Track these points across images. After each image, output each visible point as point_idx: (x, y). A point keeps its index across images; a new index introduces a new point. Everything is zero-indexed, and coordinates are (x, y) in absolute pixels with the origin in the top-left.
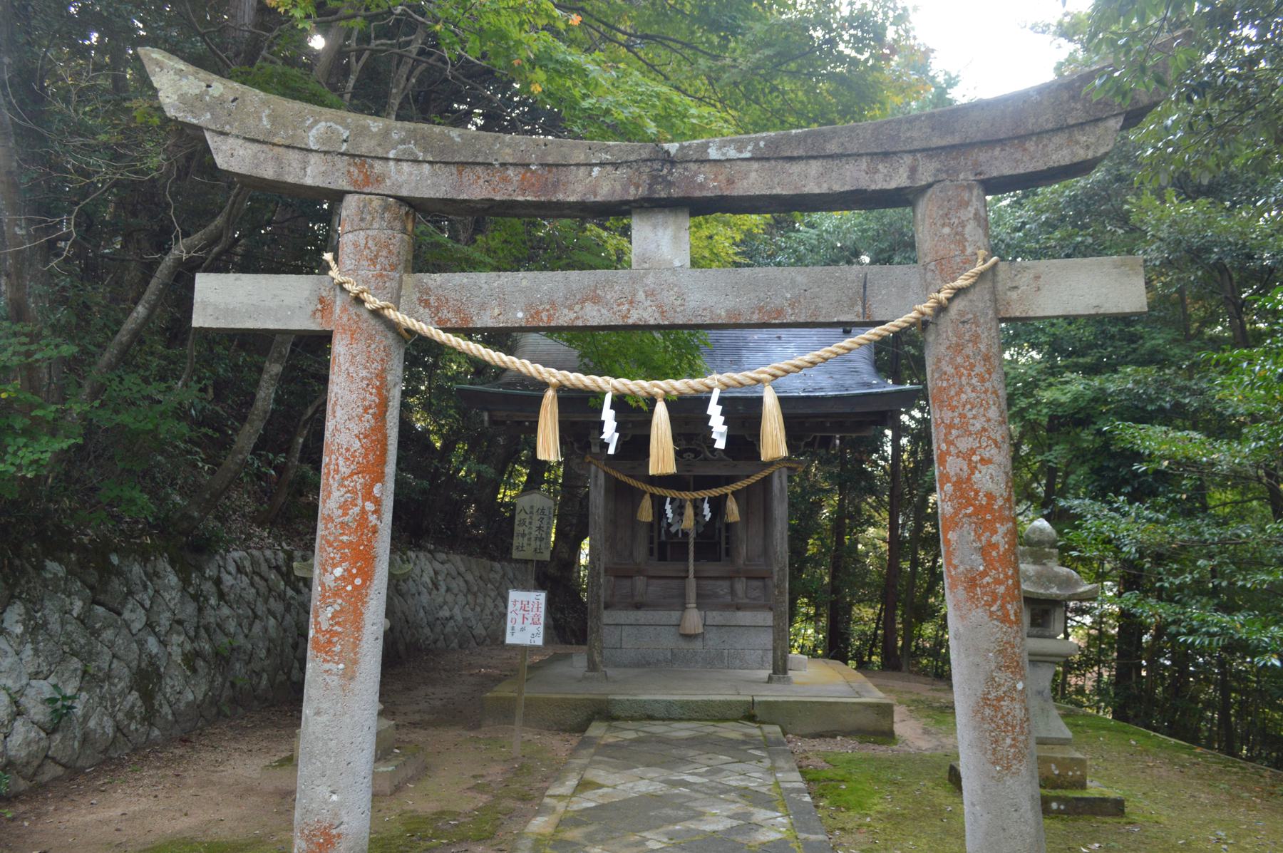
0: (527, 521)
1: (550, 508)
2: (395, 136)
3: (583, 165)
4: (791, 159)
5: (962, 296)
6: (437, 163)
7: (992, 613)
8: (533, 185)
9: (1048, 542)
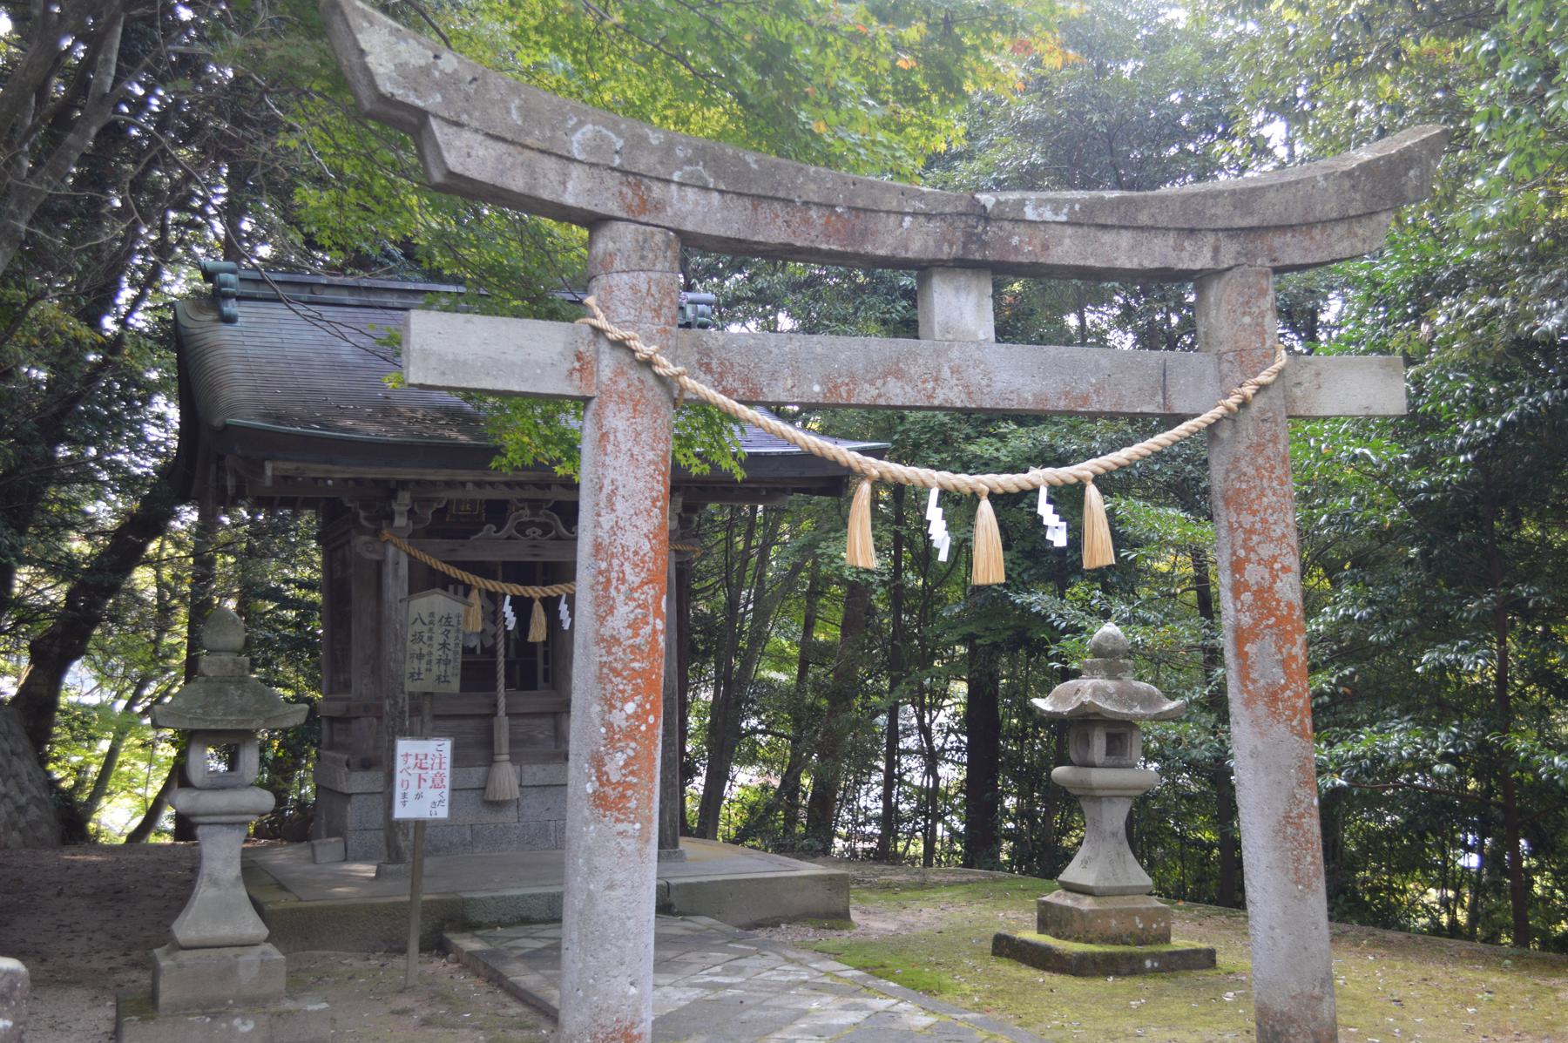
0: (426, 635)
1: (458, 616)
2: (680, 154)
3: (895, 213)
4: (1104, 227)
5: (1263, 392)
6: (728, 192)
7: (1293, 727)
8: (838, 231)
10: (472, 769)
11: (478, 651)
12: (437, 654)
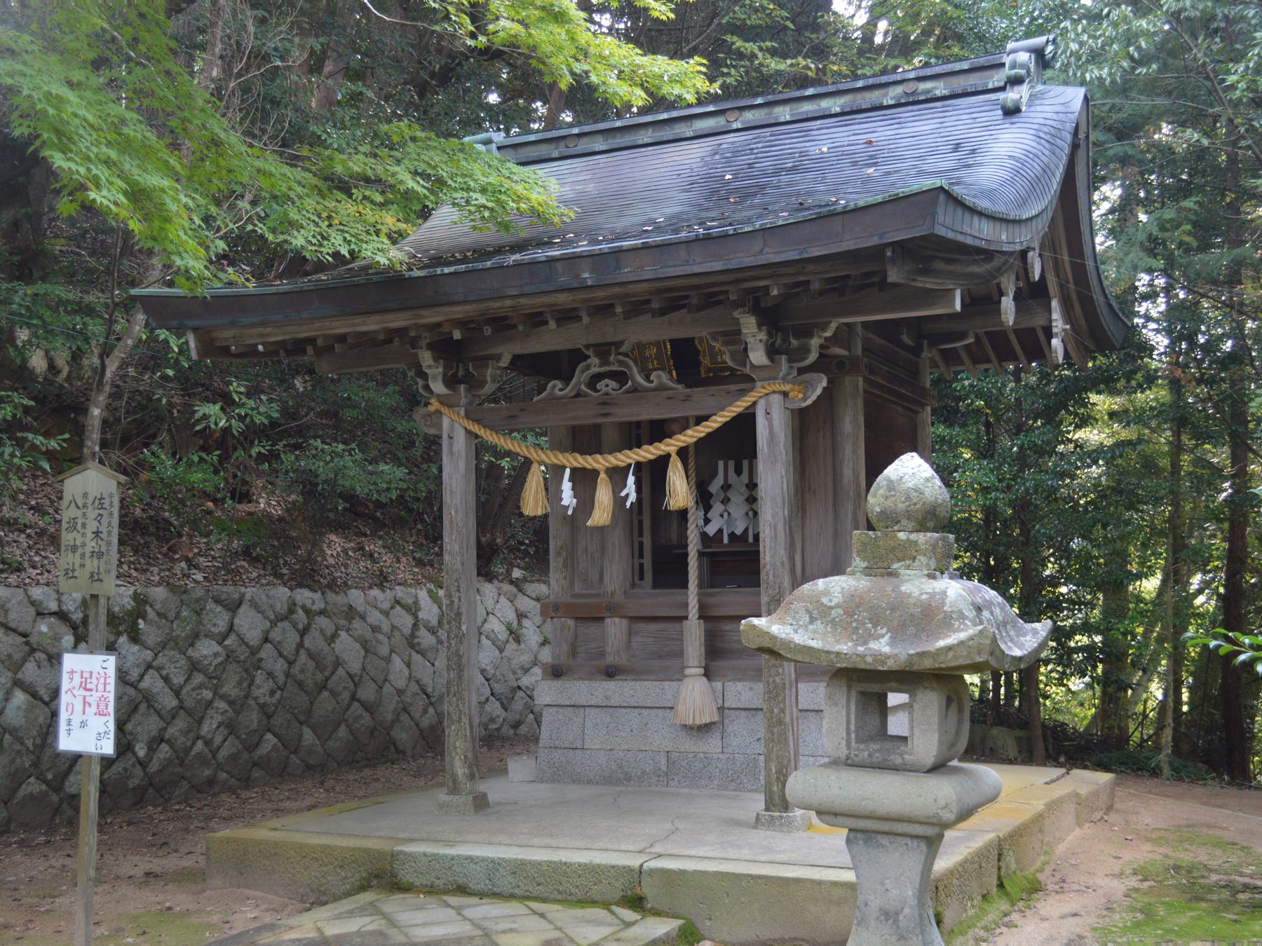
0: (80, 521)
9: (908, 515)
10: (666, 683)
11: (726, 540)
12: (91, 545)
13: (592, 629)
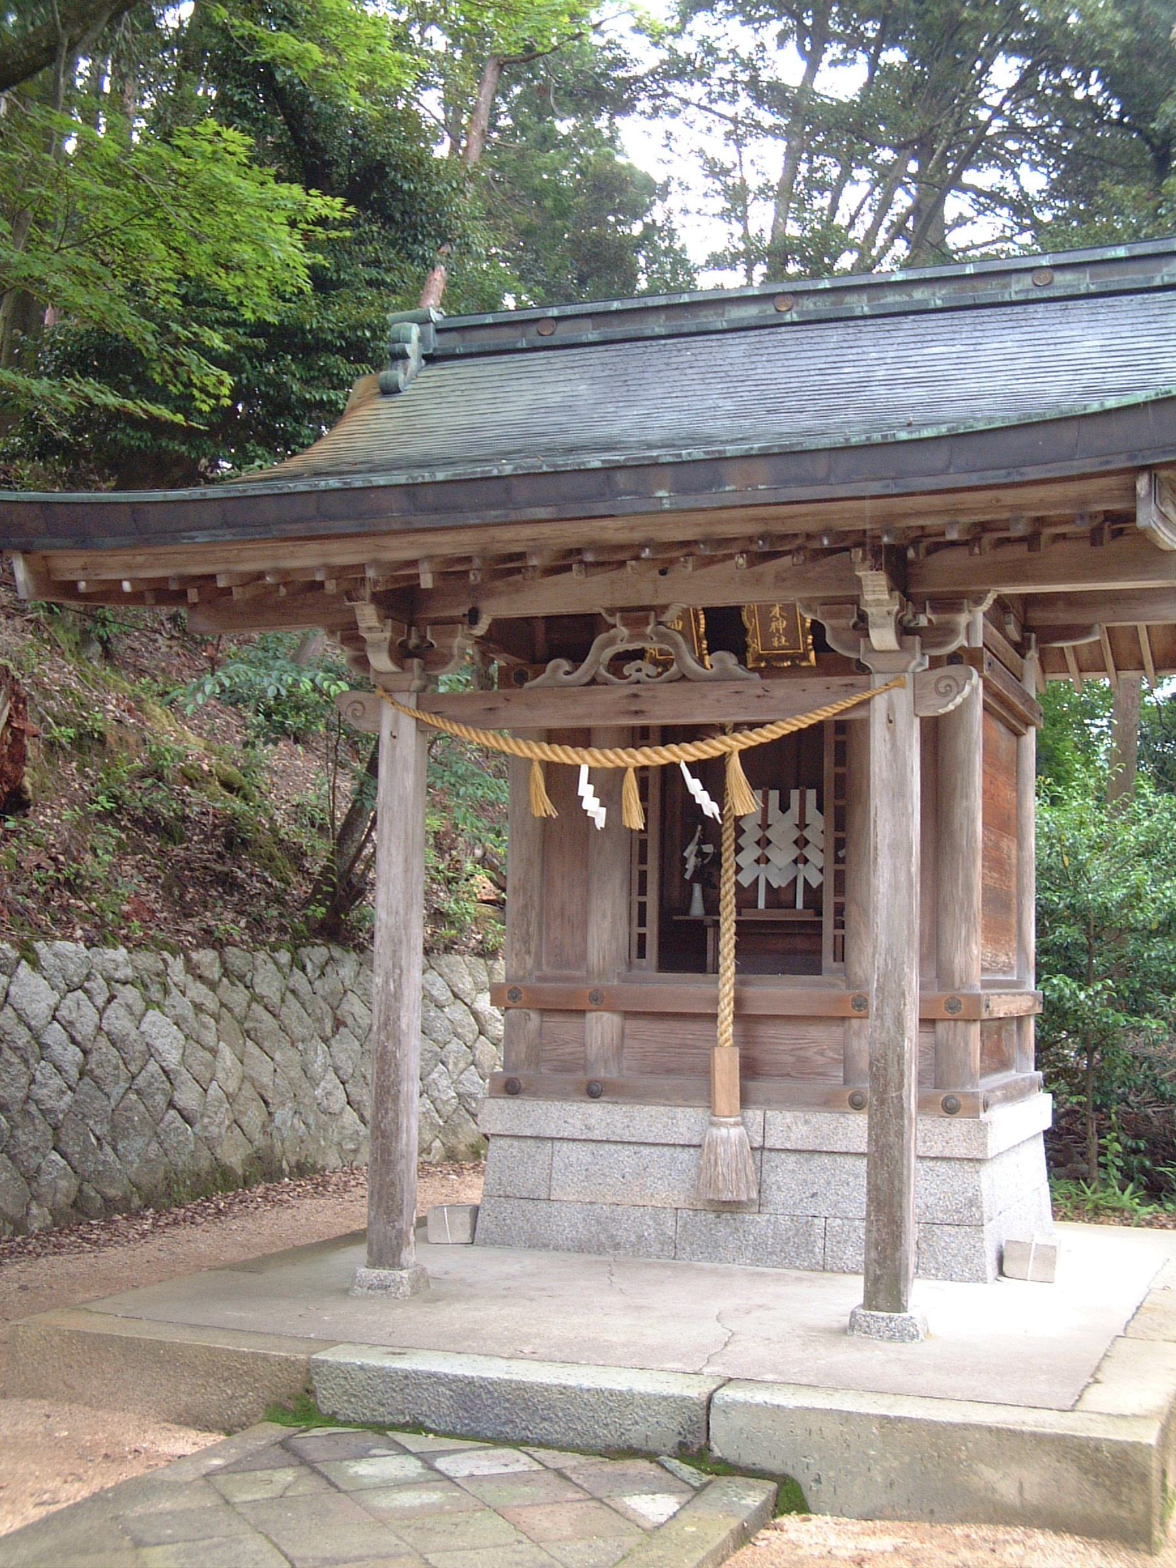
13: (562, 1027)
